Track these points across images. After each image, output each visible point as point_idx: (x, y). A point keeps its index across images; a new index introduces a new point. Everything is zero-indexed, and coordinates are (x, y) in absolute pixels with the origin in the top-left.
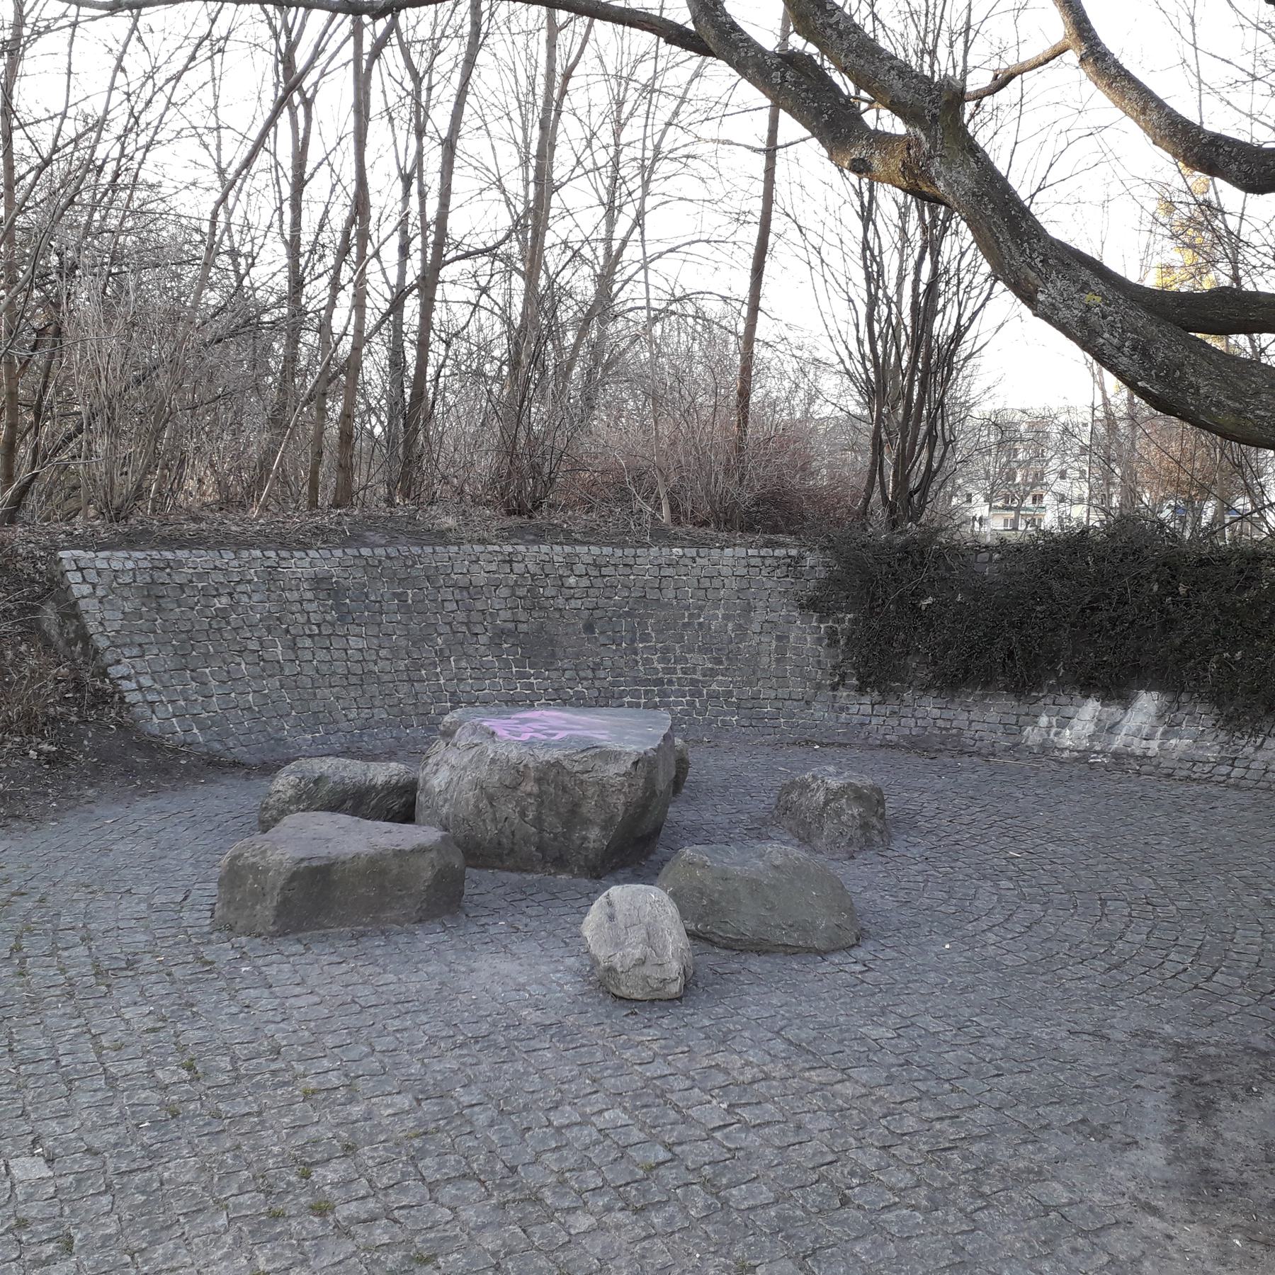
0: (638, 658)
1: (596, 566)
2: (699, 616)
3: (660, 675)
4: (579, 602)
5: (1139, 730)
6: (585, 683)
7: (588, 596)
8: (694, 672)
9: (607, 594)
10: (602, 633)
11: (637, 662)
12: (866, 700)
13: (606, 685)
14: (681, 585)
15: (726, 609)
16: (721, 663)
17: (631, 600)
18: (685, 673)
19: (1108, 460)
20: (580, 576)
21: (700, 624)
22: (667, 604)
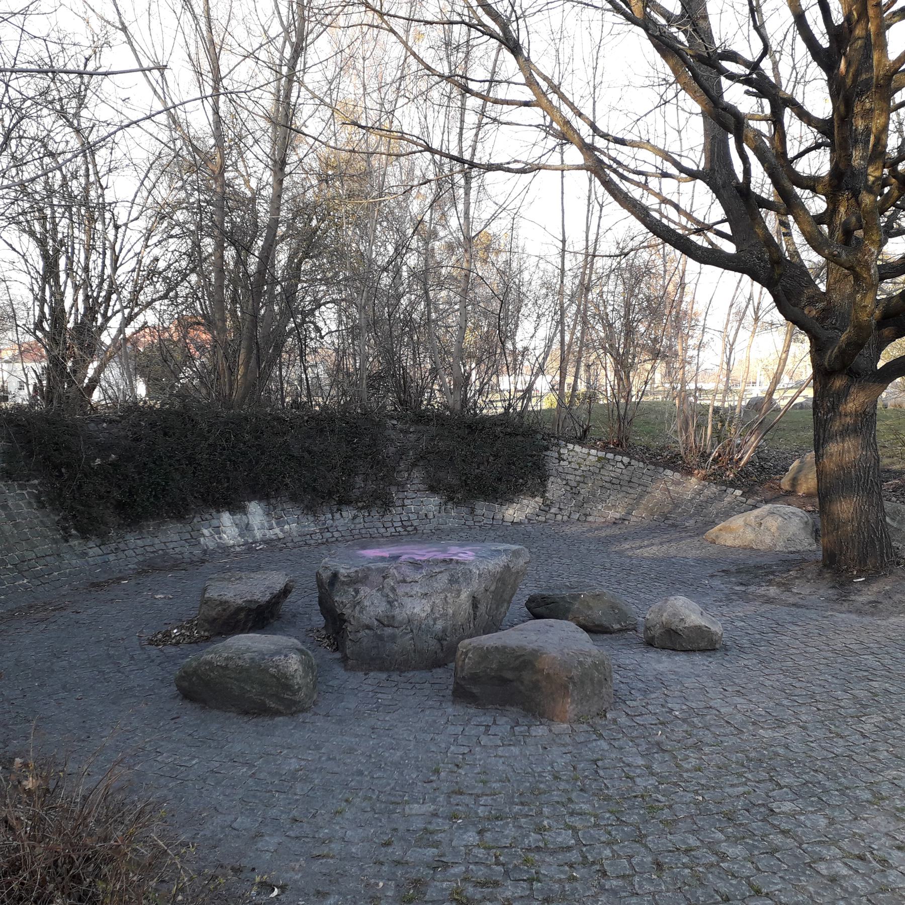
5: (263, 524)
12: (91, 544)
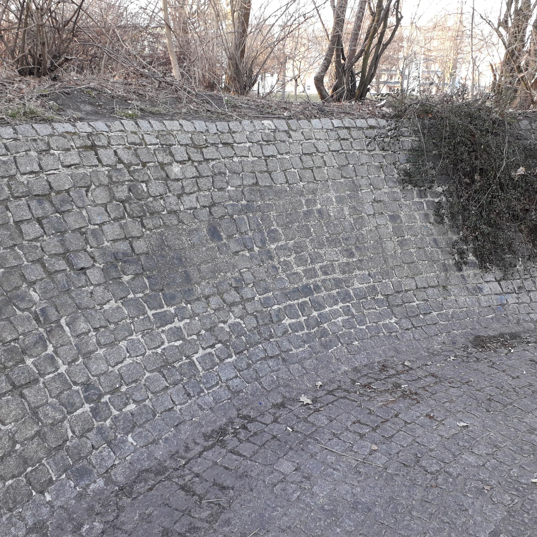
0: (276, 263)
4: (193, 197)
6: (236, 309)
7: (199, 190)
8: (334, 271)
10: (230, 237)
11: (277, 269)
21: (320, 211)
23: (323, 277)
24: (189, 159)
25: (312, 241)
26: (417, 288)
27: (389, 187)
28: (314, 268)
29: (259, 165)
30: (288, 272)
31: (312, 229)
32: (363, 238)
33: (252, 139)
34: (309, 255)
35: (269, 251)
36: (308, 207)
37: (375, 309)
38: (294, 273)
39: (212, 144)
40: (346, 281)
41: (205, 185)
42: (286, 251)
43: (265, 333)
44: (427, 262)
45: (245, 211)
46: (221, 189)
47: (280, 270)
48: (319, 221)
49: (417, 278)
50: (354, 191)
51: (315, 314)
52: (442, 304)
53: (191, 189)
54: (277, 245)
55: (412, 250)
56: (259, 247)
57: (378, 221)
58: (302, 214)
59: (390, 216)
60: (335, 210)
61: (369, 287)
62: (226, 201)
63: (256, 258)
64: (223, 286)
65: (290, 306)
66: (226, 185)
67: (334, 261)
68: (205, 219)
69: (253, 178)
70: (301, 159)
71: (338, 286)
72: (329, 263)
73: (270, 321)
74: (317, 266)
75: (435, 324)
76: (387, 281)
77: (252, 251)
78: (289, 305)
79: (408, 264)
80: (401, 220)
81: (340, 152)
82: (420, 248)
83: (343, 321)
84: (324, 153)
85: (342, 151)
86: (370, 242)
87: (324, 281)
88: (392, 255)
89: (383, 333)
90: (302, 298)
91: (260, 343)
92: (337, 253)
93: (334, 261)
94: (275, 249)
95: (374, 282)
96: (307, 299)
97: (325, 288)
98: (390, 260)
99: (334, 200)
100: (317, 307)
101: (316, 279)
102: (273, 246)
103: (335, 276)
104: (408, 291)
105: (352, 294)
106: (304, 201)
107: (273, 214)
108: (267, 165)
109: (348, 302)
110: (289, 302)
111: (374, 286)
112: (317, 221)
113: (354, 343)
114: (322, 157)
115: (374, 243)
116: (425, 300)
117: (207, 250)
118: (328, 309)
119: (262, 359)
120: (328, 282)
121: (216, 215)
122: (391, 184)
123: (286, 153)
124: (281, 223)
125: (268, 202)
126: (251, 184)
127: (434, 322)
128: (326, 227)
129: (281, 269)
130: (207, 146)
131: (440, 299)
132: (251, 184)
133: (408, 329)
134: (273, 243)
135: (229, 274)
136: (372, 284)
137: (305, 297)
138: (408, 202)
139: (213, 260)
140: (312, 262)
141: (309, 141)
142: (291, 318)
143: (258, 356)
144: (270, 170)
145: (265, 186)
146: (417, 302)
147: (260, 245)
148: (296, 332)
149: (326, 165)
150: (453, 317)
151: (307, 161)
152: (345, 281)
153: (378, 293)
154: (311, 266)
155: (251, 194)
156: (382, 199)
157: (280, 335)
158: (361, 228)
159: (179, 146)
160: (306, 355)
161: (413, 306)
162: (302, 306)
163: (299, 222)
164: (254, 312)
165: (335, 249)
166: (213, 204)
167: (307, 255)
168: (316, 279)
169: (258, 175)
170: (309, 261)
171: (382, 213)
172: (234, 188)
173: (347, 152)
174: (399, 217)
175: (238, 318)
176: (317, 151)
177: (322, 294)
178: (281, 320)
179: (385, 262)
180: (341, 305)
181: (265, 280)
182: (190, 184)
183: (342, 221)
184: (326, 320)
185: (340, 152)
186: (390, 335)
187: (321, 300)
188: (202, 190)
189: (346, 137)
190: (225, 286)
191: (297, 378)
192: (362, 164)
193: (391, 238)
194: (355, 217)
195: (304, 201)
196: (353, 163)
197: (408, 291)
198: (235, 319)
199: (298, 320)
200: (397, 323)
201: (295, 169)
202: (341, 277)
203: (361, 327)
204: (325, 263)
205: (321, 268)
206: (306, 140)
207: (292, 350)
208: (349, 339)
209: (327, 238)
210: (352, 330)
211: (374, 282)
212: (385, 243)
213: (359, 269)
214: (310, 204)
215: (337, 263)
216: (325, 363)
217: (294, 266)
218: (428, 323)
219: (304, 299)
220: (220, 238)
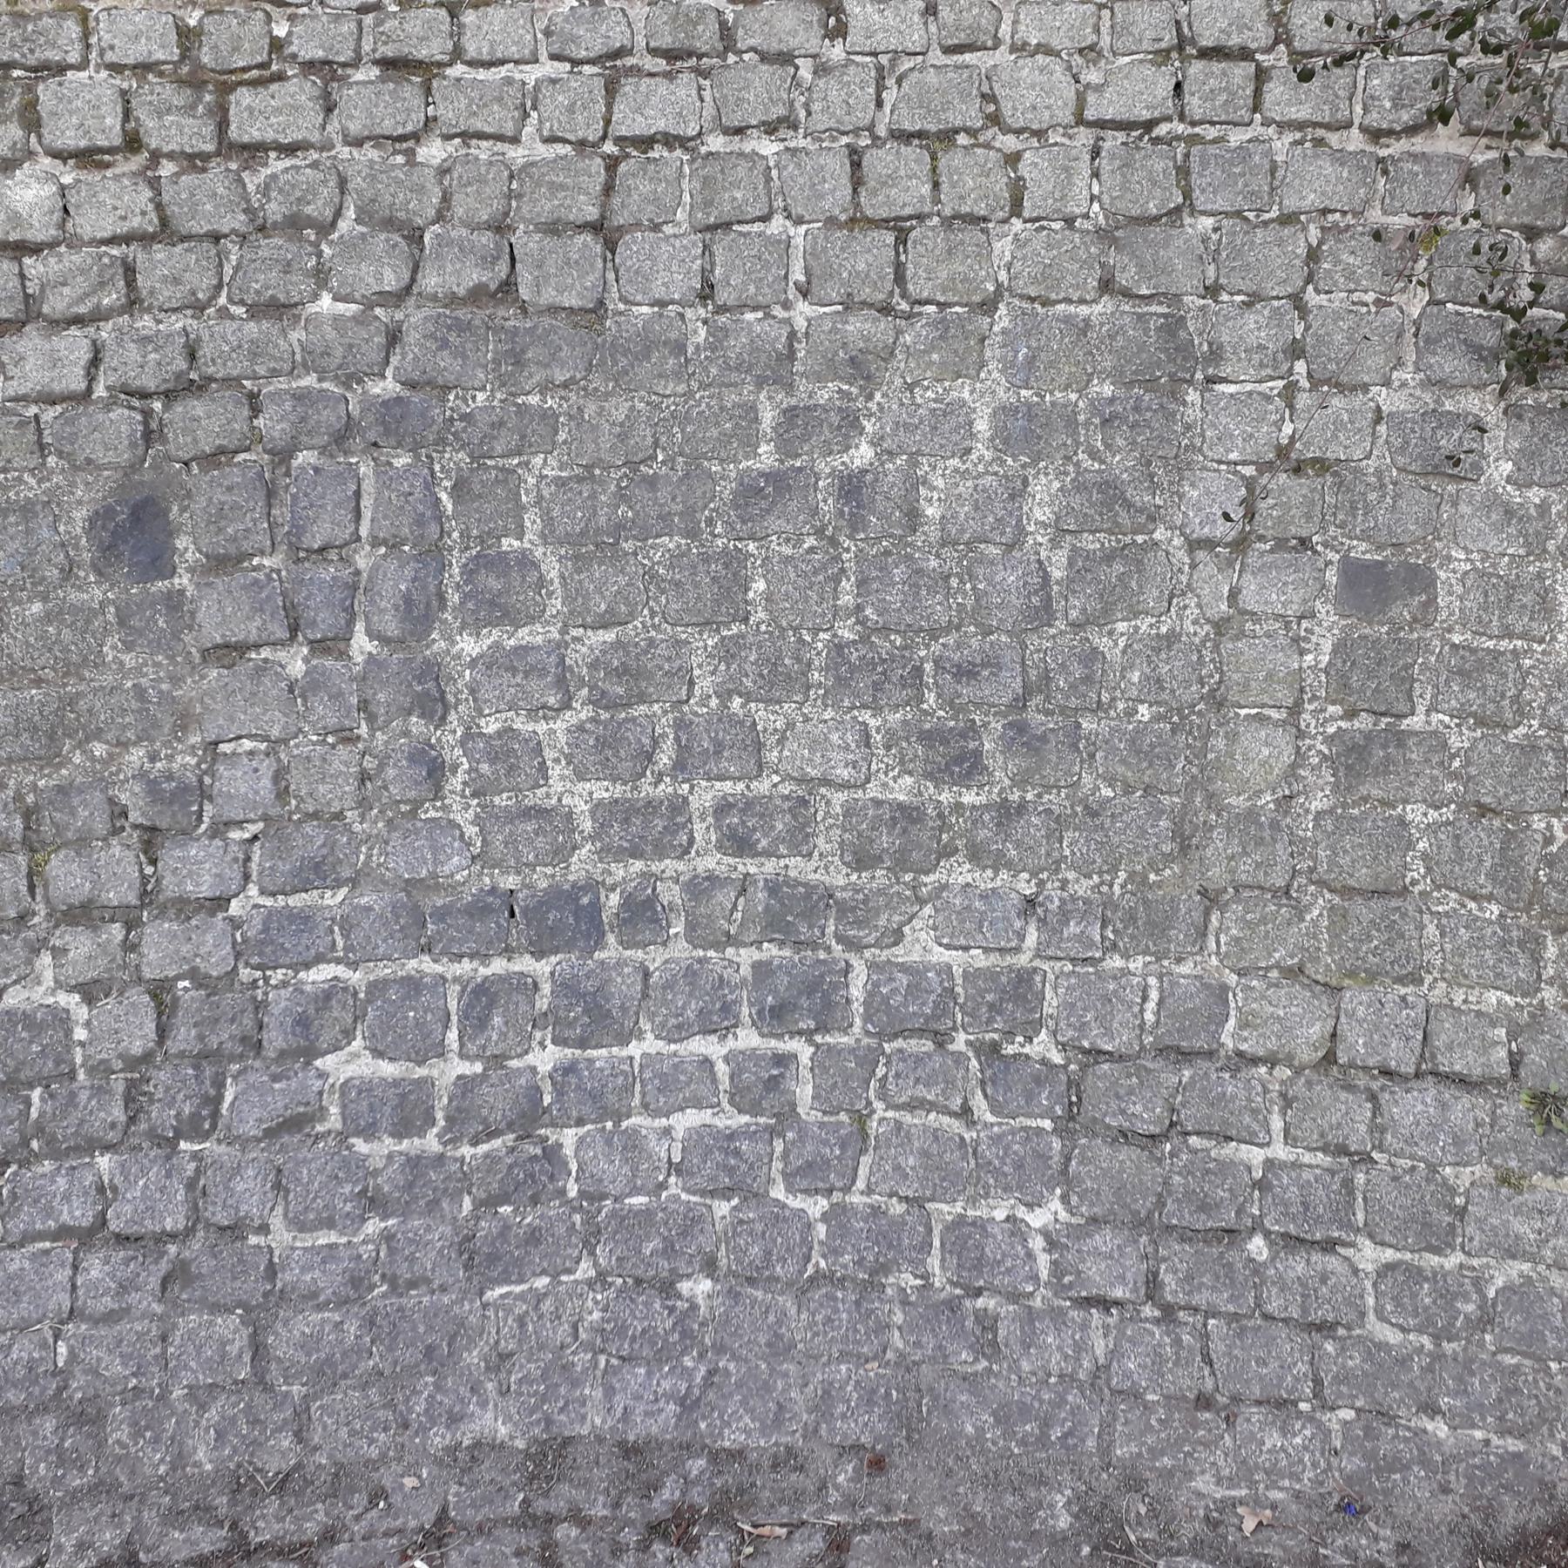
0: (449, 738)
1: (194, 82)
2: (850, 423)
3: (582, 863)
4: (74, 346)
6: (80, 944)
7: (133, 303)
8: (799, 840)
9: (265, 283)
10: (221, 563)
11: (436, 771)
13: (215, 958)
14: (739, 196)
15: (1025, 372)
16: (968, 767)
17: (414, 317)
18: (739, 844)
19: (1416, 1434)
20: (88, 158)
21: (852, 487)
22: (647, 344)
23: (711, 862)
24: (133, 143)
25: (728, 652)
26: (1330, 1058)
27: (1429, 383)
28: (679, 806)
29: (562, 187)
30: (503, 800)
31: (760, 585)
32: (1087, 680)
33: (574, 39)
34: (680, 725)
35: (432, 671)
36: (786, 448)
37: (965, 1113)
38: (540, 812)
39: (309, 66)
40: (856, 911)
41: (176, 281)
42: (534, 684)
43: (170, 1105)
44: (1494, 910)
45: (372, 436)
46: (276, 309)
47: (456, 782)
48: (833, 542)
49: (1357, 1000)
50: (1150, 384)
51: (545, 1058)
52: (1462, 1212)
53: (81, 300)
54: (497, 645)
55: (1415, 813)
56: (384, 640)
57: (1250, 586)
58: (726, 490)
59: (1353, 573)
60: (965, 487)
61: (991, 975)
62: (275, 373)
63: (337, 696)
64: (73, 813)
65: (413, 985)
66: (306, 286)
67: (825, 782)
68: (111, 457)
69: (490, 261)
70: (856, 165)
71: (788, 929)
72: (785, 789)
73: (244, 1040)
74: (703, 796)
75: (1325, 1328)
76: (1137, 964)
77: (327, 651)
78: (408, 980)
79: (1347, 892)
80: (1432, 600)
81: (1162, 130)
82: (1484, 810)
83: (698, 1140)
84: (1039, 134)
85: (1180, 128)
86: (1131, 713)
87: (700, 887)
88: (1251, 815)
89: (925, 1277)
90: (509, 952)
91: (108, 1148)
92: (866, 739)
93: (825, 782)
94: (473, 663)
95: (1038, 956)
96: (541, 968)
97: (691, 927)
98: (1219, 845)
99: (982, 426)
100: (571, 1024)
101: (656, 867)
102: (469, 646)
103: (796, 866)
104: (1255, 1061)
105: (857, 992)
106: (768, 417)
107: (545, 466)
108: (608, 189)
109: (808, 1035)
110: (426, 965)
111: (1024, 978)
112: (810, 542)
113: (684, 1287)
114: (1013, 159)
115: (1157, 718)
116: (1342, 1150)
117: (48, 618)
118: (647, 1045)
119: (63, 1233)
120: (725, 897)
121: (179, 443)
122: (1450, 364)
123: (770, 128)
124: (564, 526)
125: (534, 400)
126: (461, 292)
127: (1316, 1315)
128: (861, 583)
129: (461, 777)
130: (280, 77)
131: (1464, 1177)
132: (461, 292)
133: (1105, 1304)
134: (475, 626)
135: (136, 755)
136: (1023, 960)
137: (539, 954)
138: (1535, 495)
139: (70, 670)
140: (679, 766)
141: (968, 57)
142: (378, 1054)
143: (49, 1212)
144: (619, 220)
145: (553, 310)
146: (1280, 1151)
147: (392, 628)
148: (358, 1133)
149: (1016, 207)
150: (1485, 1320)
151: (890, 180)
152: (843, 910)
153: (1038, 1025)
154: (665, 788)
155: (444, 344)
156: (1335, 452)
157: (250, 1128)
158: (1101, 618)
159: (104, 74)
160: (328, 1281)
161: (1226, 1168)
162: (482, 998)
163: (692, 534)
164: (179, 978)
165: (865, 715)
166: (178, 390)
167: (665, 725)
168: (656, 867)
169: (526, 241)
170: (664, 759)
171: (1304, 543)
172: (352, 308)
173: (1212, 132)
174: (1421, 580)
175: (71, 990)
176: (995, 119)
177: (655, 958)
178: (310, 1053)
179: (1185, 849)
180: (748, 1038)
181: (339, 816)
182: (82, 272)
183: (982, 560)
184: (586, 1110)
185: (1162, 130)
186: (953, 1305)
187: (625, 986)
188: (149, 310)
189: (1235, 41)
190: (89, 814)
191: (178, 1393)
192: (1287, 219)
193: (1295, 710)
194: (1090, 543)
195: (768, 417)
196: (1221, 204)
197: (1255, 1061)
198: (53, 992)
199: (421, 1072)
200: (1052, 1244)
201: (799, 221)
202: (839, 878)
203: (795, 1202)
204: (762, 786)
205: (723, 808)
206: (949, 50)
207: (264, 1229)
208: (669, 1250)
209: (839, 647)
210: (722, 1208)
211: (1038, 956)
212: (1233, 737)
213: (976, 855)
214: (805, 438)
215: (839, 798)
216: (411, 1356)
217: (555, 772)
218: (1273, 1307)
219: (525, 964)
220: (159, 563)
